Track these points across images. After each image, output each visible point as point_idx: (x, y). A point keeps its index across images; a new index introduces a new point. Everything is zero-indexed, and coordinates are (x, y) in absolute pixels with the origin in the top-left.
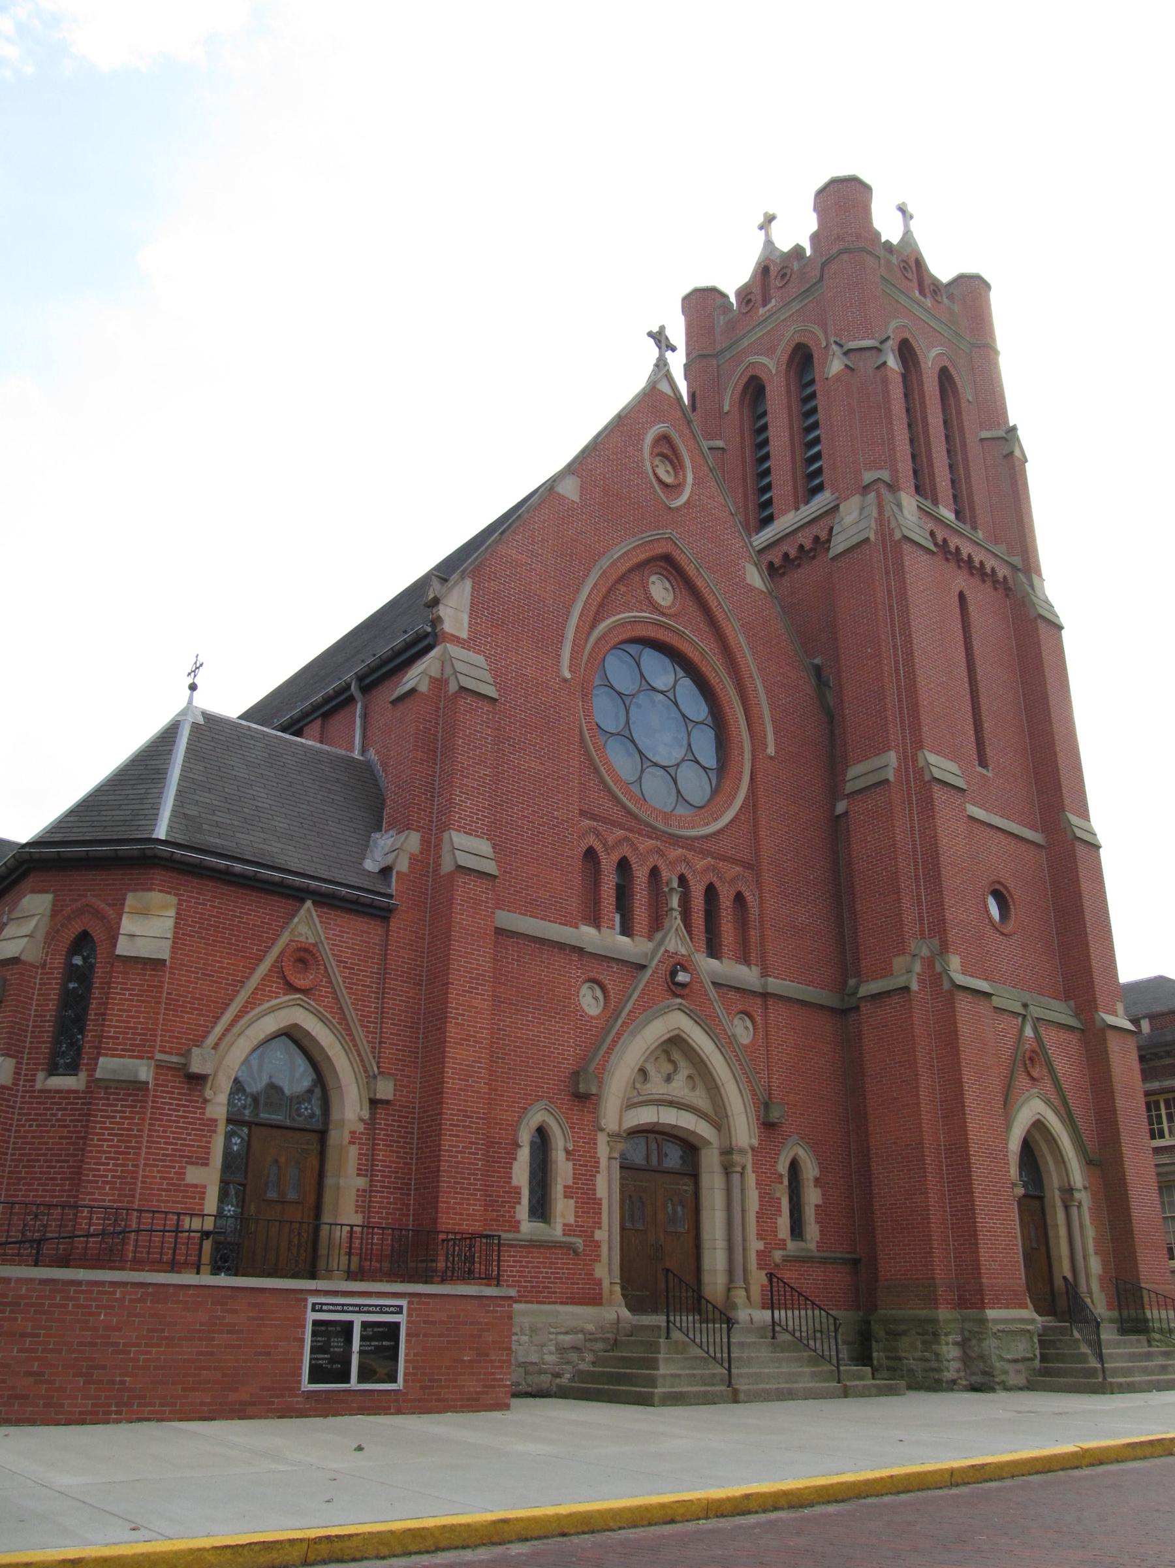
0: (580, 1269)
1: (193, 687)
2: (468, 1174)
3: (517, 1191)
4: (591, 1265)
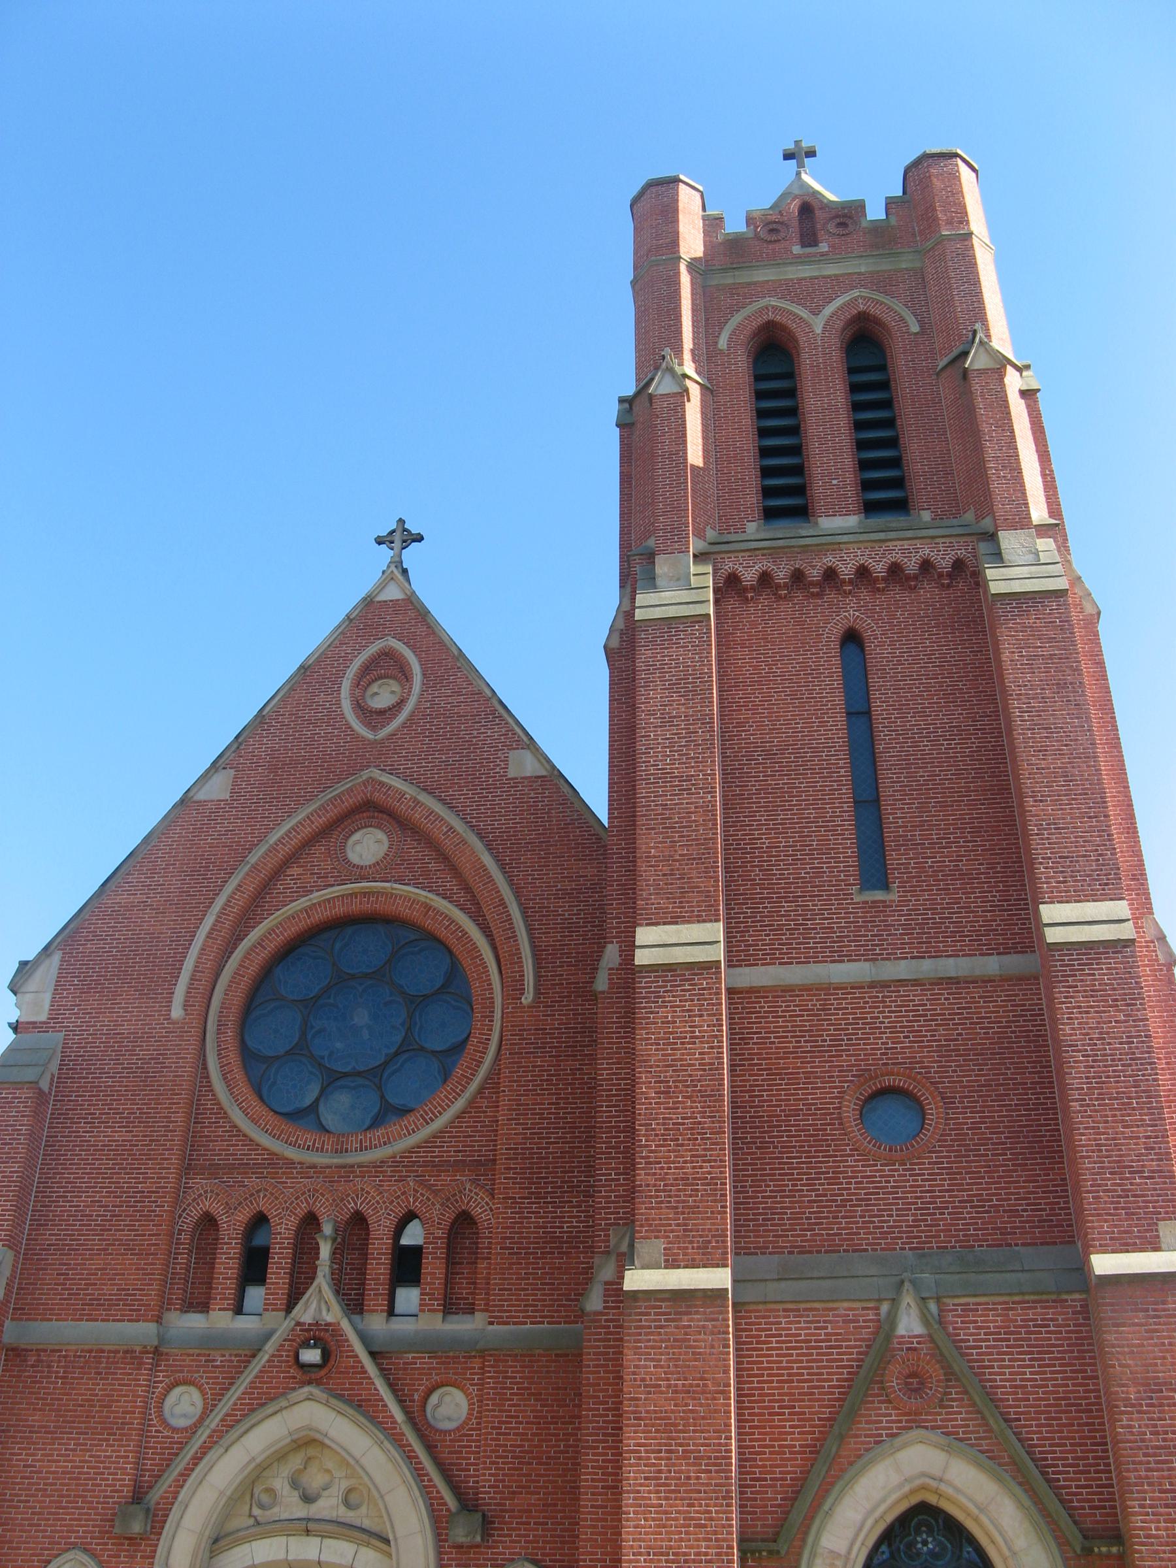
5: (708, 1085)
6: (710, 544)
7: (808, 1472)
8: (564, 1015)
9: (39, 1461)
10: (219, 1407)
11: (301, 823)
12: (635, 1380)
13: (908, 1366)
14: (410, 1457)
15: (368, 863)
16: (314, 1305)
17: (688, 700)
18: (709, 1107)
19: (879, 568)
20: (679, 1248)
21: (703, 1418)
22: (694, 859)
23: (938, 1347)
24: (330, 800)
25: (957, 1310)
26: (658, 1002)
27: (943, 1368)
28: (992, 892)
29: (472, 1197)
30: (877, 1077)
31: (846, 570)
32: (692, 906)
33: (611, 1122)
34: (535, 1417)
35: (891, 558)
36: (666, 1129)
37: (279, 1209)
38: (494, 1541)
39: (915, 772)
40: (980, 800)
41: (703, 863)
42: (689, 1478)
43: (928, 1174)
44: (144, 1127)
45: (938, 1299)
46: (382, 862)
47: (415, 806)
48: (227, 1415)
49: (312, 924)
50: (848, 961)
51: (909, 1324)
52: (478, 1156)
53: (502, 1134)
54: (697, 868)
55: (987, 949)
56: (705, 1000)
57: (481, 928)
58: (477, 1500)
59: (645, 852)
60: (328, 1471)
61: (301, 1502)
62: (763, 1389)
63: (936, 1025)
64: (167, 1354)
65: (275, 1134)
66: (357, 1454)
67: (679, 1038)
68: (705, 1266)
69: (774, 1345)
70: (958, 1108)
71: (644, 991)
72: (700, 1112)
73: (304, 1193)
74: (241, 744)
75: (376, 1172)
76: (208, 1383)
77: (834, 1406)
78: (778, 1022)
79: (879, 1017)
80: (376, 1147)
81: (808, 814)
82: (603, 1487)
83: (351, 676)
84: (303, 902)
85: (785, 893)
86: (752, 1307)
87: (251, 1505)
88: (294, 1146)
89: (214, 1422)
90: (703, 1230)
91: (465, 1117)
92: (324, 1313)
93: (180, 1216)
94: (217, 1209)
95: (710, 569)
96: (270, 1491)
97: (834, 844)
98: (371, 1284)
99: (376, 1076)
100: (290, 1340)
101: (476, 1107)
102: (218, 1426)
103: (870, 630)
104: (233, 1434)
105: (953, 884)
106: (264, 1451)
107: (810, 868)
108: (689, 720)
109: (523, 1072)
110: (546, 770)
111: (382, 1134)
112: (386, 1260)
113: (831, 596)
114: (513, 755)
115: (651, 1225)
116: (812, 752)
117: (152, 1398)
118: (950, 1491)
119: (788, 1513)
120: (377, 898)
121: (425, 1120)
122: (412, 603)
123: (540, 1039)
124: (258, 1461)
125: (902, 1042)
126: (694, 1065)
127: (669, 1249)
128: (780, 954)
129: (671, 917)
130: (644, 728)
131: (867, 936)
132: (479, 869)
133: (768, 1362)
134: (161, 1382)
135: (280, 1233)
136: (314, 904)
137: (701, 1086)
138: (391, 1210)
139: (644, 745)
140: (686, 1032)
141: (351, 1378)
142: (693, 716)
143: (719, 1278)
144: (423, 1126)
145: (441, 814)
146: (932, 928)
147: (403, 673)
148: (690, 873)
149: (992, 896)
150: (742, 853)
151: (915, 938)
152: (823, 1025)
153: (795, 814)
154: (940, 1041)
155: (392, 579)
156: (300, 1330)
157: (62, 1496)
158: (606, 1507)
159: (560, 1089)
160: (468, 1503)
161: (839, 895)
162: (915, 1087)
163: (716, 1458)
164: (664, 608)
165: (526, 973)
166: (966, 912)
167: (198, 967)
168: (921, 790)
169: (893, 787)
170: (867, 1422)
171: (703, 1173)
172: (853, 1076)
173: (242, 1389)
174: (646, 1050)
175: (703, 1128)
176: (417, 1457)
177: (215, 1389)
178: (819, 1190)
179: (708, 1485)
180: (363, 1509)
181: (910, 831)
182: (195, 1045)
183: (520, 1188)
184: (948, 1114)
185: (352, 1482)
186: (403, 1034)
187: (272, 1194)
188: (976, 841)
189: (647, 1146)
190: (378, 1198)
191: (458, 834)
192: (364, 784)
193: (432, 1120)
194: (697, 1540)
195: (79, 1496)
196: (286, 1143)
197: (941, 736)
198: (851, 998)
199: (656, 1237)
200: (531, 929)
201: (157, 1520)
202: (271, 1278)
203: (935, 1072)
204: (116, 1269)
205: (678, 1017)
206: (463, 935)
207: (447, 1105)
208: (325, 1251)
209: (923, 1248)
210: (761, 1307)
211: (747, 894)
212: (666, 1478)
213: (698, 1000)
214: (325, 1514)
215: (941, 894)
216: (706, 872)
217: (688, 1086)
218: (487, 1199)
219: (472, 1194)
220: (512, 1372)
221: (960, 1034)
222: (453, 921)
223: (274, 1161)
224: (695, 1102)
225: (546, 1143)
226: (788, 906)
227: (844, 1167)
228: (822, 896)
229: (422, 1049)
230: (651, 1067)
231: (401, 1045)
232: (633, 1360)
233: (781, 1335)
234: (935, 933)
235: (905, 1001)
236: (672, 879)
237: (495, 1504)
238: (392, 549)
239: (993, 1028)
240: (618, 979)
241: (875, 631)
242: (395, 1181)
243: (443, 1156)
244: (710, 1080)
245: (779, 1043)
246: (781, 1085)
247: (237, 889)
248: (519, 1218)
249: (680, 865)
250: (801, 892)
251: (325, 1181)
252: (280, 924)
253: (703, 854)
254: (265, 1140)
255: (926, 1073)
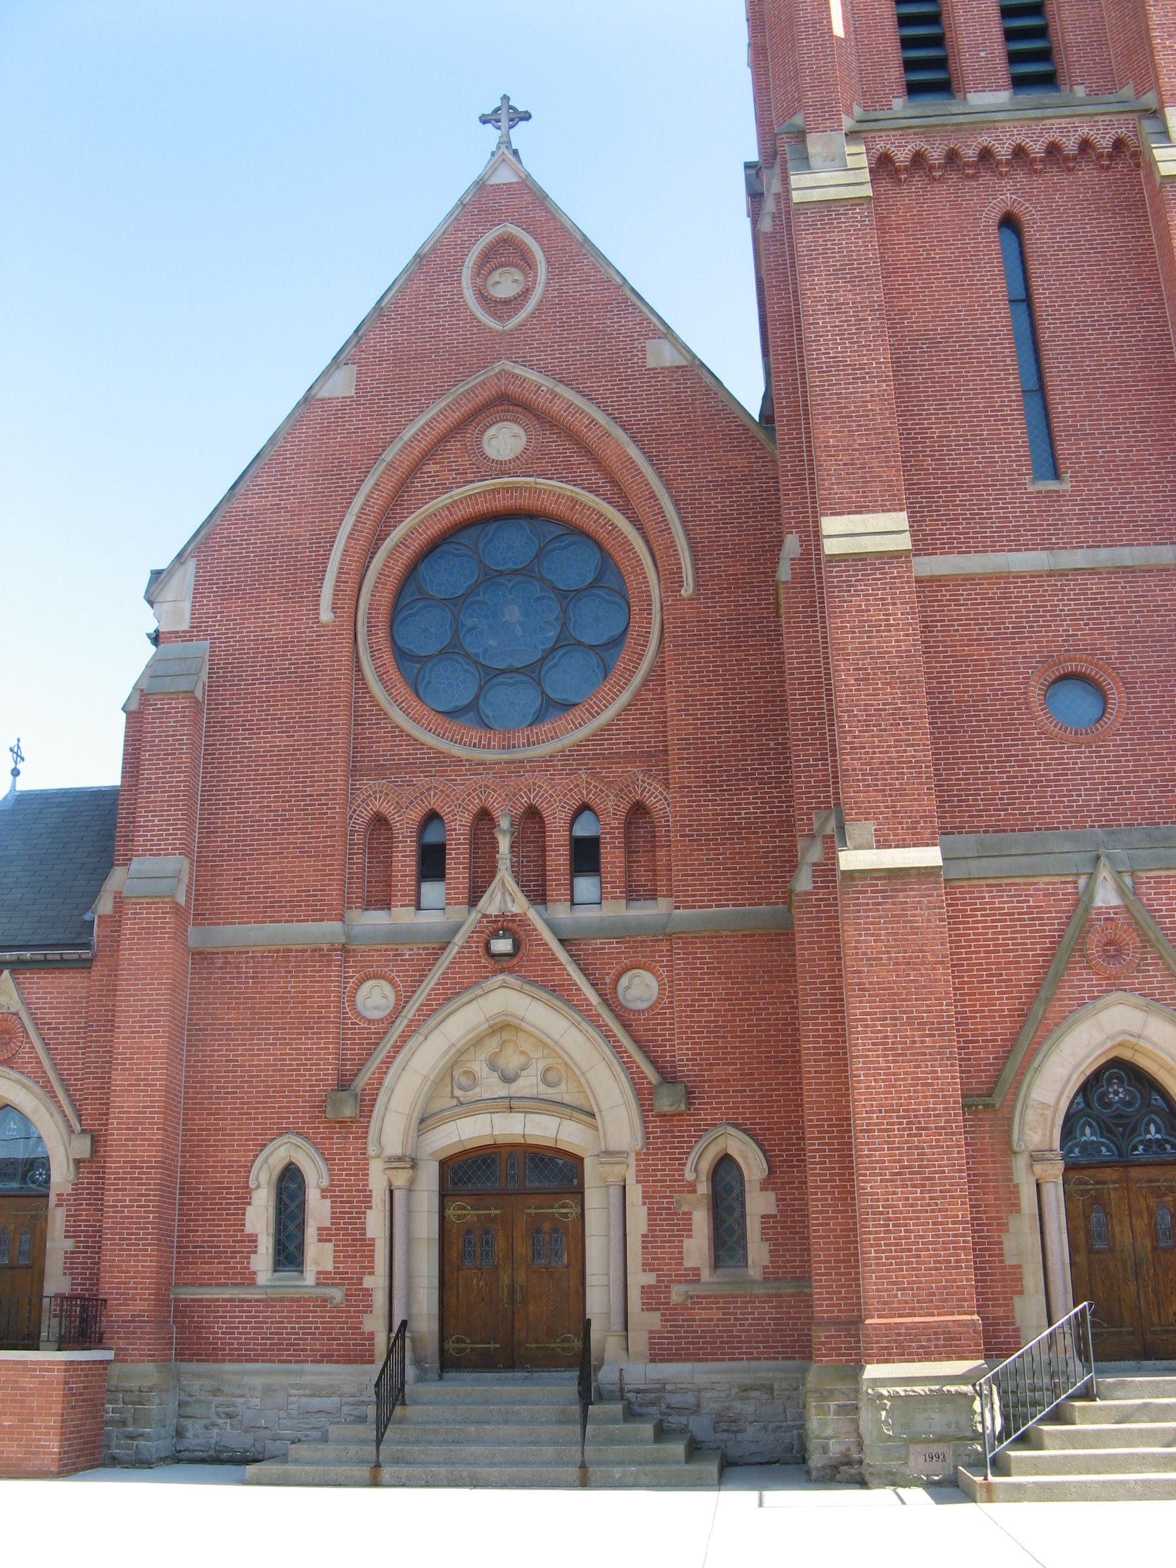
0: (343, 1323)
1: (16, 773)
2: (137, 1228)
3: (253, 1240)
4: (358, 1317)
5: (906, 672)
6: (858, 122)
7: (1018, 1033)
8: (725, 606)
9: (240, 1055)
10: (414, 998)
11: (434, 419)
12: (857, 954)
13: (1106, 935)
14: (608, 1036)
15: (507, 458)
16: (498, 898)
17: (854, 286)
18: (909, 693)
19: (1037, 149)
20: (889, 829)
21: (924, 987)
22: (874, 448)
23: (1133, 917)
24: (463, 394)
25: (1150, 883)
26: (850, 591)
27: (1139, 936)
28: (1163, 482)
29: (646, 788)
30: (1060, 663)
31: (1003, 151)
32: (876, 496)
33: (805, 710)
34: (726, 994)
35: (1048, 137)
36: (867, 715)
37: (451, 806)
38: (695, 1109)
39: (1082, 362)
40: (1147, 390)
41: (883, 453)
42: (914, 1042)
43: (1113, 756)
44: (305, 731)
45: (1133, 873)
46: (522, 456)
47: (553, 399)
48: (423, 1005)
49: (455, 521)
50: (1026, 550)
51: (1106, 896)
52: (648, 747)
53: (672, 725)
54: (878, 458)
55: (1160, 539)
56: (897, 588)
57: (631, 521)
58: (675, 1072)
59: (823, 442)
60: (523, 1053)
61: (501, 1082)
62: (971, 959)
63: (1114, 613)
64: (354, 951)
65: (439, 733)
66: (556, 1037)
67: (874, 626)
68: (915, 845)
69: (979, 918)
70: (1139, 692)
71: (835, 580)
72: (899, 698)
73: (475, 790)
74: (360, 338)
75: (547, 766)
76: (399, 976)
77: (1039, 973)
78: (961, 610)
79: (1058, 606)
80: (543, 742)
81: (977, 403)
82: (825, 1054)
83: (471, 265)
84: (443, 500)
85: (958, 482)
86: (957, 883)
87: (452, 1087)
88: (460, 744)
89: (410, 1012)
90: (911, 811)
91: (631, 710)
92: (510, 904)
93: (351, 817)
94: (387, 808)
95: (863, 149)
96: (469, 1073)
97: (1004, 434)
98: (552, 875)
99: (533, 672)
100: (477, 932)
101: (642, 700)
102: (415, 1016)
103: (1030, 216)
104: (432, 1022)
105: (1124, 475)
106: (462, 1038)
107: (983, 458)
108: (857, 307)
109: (688, 663)
110: (686, 359)
111: (549, 728)
112: (564, 851)
113: (987, 178)
114: (650, 345)
115: (860, 808)
116: (976, 341)
117: (344, 993)
118: (1149, 1046)
119: (1000, 1070)
120: (521, 493)
121: (591, 713)
122: (527, 186)
123: (702, 630)
124: (458, 1046)
125: (1082, 630)
126: (891, 652)
127: (880, 830)
128: (957, 543)
129: (856, 507)
130: (812, 315)
131: (1042, 525)
132: (625, 462)
133: (975, 934)
134: (352, 977)
135: (455, 830)
136: (455, 502)
137: (900, 673)
138: (565, 803)
139: (813, 332)
140: (881, 620)
141: (543, 965)
142: (860, 302)
143: (930, 856)
144: (590, 720)
145: (580, 405)
146: (1106, 518)
147: (525, 261)
148: (871, 463)
149: (1163, 487)
150: (913, 443)
151: (1090, 528)
152: (1005, 613)
153: (963, 403)
154: (1119, 628)
155: (503, 160)
156: (487, 922)
157: (268, 1086)
158: (829, 1072)
159: (727, 679)
160: (668, 1077)
161: (1013, 485)
162: (1097, 673)
163: (939, 1023)
164: (822, 190)
165: (683, 566)
166: (1138, 502)
167: (343, 568)
168: (1089, 379)
169: (1060, 376)
170: (1070, 987)
171: (907, 757)
172: (1036, 662)
173: (435, 980)
174: (843, 638)
175: (904, 714)
176: (614, 1036)
177: (407, 981)
178: (1009, 772)
179: (932, 1047)
180: (563, 1086)
181: (1080, 421)
182: (349, 647)
183: (695, 777)
184: (1129, 698)
185: (549, 1062)
186: (559, 629)
187: (442, 792)
188: (1146, 432)
189: (850, 732)
190: (600, 787)
191: (600, 426)
192: (496, 376)
193: (598, 714)
194: (925, 1097)
195: (285, 1086)
196: (451, 741)
197: (1105, 325)
198: (1031, 587)
199: (866, 819)
200: (684, 522)
201: (367, 1104)
202: (450, 873)
203: (1116, 658)
204: (294, 872)
205: (872, 605)
206: (613, 529)
207: (612, 698)
208: (504, 844)
209: (1112, 826)
210: (965, 883)
211: (921, 484)
212: (893, 1043)
213: (890, 588)
214: (526, 1092)
215: (1113, 484)
216: (887, 462)
217: (886, 673)
218: (661, 789)
219: (646, 785)
220: (701, 953)
221: (1138, 622)
222: (602, 515)
223: (440, 758)
224: (894, 688)
225: (718, 733)
226: (963, 496)
227: (1033, 749)
228: (996, 485)
229: (580, 644)
230: (848, 654)
231: (557, 642)
232: (854, 936)
233: (985, 909)
234: (1109, 522)
235: (1082, 589)
236: (853, 469)
237: (694, 1076)
238: (499, 128)
239: (1170, 615)
240: (800, 569)
241: (1033, 215)
242: (566, 774)
243: (612, 749)
244: (907, 667)
245: (963, 630)
246: (967, 671)
247: (374, 488)
248: (696, 806)
249: (860, 454)
250: (975, 481)
251: (496, 777)
252: (422, 522)
253: (883, 443)
254: (430, 739)
255: (1107, 659)
